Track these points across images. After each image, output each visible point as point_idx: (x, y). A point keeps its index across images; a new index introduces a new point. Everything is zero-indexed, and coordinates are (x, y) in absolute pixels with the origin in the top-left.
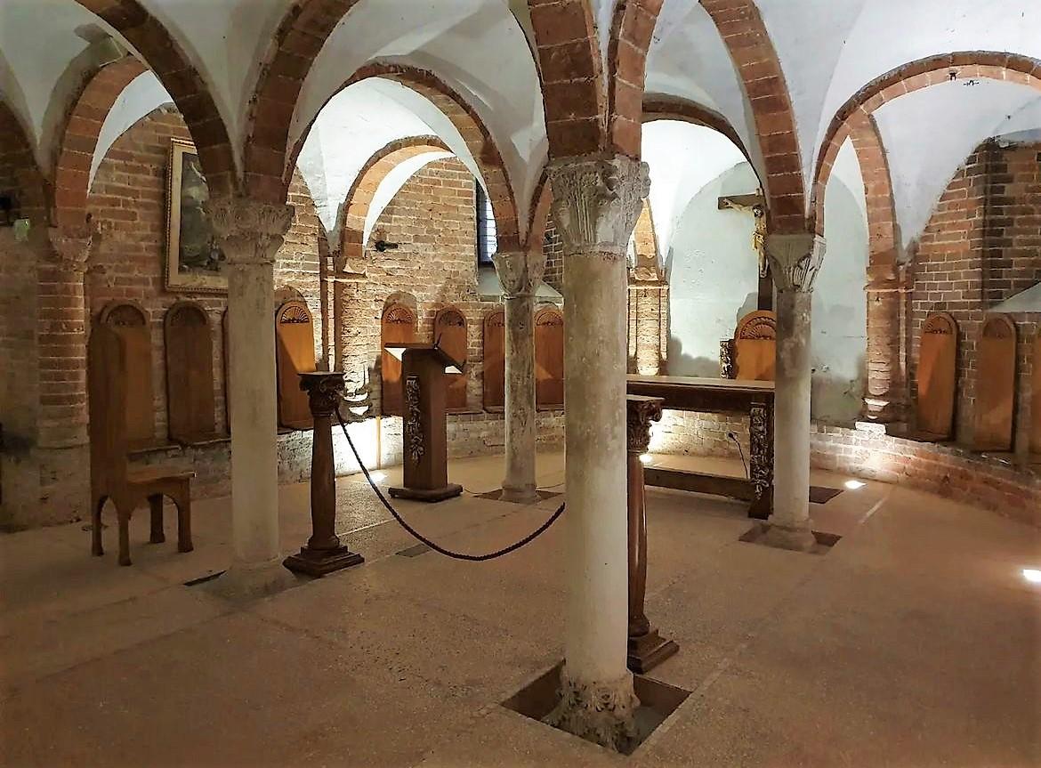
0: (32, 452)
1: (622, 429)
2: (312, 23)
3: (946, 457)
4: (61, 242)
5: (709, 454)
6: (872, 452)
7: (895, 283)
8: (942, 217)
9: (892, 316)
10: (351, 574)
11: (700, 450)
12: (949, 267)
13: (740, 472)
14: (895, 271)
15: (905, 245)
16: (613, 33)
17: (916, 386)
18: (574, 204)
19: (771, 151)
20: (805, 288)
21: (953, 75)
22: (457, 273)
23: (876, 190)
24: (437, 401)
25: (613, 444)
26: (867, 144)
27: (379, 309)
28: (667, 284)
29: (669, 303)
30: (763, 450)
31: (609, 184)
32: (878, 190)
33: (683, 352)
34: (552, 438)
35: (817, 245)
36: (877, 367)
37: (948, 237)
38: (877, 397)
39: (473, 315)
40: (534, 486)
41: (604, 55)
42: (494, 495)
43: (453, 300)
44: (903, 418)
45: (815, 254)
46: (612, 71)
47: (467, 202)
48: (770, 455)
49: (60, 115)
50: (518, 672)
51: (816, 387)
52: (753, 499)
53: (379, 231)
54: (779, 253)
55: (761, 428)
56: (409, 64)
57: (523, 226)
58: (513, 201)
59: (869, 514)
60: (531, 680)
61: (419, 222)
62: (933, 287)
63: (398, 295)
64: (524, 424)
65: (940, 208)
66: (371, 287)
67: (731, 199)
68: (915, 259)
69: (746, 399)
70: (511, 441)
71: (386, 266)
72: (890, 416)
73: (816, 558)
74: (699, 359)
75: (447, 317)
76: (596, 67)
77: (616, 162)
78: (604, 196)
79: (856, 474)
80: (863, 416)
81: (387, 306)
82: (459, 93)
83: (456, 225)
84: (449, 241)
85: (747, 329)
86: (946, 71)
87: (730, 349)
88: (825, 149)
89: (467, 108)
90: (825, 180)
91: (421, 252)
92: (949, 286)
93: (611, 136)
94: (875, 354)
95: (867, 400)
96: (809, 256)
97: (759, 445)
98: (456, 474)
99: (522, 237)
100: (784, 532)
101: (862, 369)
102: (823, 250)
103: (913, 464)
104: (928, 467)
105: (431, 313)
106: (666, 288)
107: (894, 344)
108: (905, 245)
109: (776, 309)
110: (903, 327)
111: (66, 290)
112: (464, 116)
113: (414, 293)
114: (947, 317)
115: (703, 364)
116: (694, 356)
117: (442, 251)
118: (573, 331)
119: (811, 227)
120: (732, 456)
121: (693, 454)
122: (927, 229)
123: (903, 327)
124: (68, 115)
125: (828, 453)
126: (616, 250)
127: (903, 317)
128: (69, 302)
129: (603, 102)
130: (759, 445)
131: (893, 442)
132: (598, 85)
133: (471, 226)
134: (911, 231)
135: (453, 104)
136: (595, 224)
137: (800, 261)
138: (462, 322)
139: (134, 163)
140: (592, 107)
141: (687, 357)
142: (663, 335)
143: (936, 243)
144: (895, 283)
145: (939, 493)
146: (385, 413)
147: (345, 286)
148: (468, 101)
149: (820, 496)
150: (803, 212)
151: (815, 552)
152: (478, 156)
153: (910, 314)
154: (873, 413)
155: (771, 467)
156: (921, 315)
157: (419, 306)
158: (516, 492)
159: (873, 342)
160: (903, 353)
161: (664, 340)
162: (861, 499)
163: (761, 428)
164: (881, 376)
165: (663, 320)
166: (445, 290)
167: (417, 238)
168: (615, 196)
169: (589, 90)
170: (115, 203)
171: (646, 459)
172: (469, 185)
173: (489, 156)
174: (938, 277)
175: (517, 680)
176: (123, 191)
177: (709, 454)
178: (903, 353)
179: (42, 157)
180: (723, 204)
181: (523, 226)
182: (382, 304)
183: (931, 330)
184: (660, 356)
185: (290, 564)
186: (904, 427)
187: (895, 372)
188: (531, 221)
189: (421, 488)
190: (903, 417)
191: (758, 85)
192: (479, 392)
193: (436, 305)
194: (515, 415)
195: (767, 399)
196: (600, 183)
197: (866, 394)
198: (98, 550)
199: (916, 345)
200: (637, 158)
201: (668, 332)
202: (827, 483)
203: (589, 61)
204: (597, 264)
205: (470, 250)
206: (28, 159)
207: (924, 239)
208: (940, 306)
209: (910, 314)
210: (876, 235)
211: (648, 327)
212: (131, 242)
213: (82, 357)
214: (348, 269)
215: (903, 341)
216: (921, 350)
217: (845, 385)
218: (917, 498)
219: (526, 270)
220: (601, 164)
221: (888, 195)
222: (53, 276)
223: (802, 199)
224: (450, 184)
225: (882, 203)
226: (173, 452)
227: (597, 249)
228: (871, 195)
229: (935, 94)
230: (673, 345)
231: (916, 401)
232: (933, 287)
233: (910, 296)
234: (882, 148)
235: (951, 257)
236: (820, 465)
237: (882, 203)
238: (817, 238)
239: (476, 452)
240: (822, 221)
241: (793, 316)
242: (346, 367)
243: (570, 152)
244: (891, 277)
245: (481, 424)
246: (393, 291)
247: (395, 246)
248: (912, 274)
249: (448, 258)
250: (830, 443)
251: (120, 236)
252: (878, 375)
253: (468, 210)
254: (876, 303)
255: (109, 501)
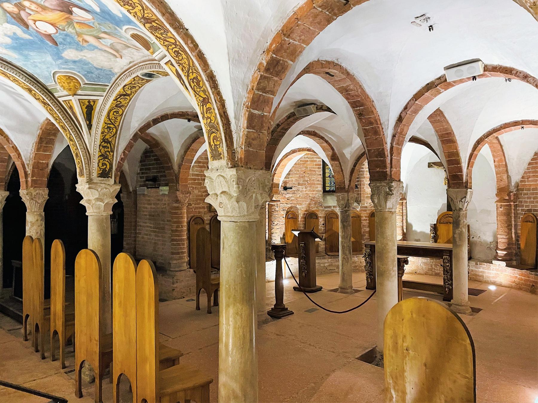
0: (168, 272)
1: (396, 268)
2: (283, 129)
3: (532, 276)
4: (180, 195)
5: (426, 274)
6: (500, 275)
7: (509, 201)
8: (529, 172)
9: (508, 214)
10: (290, 317)
11: (422, 272)
12: (533, 194)
13: (440, 282)
14: (509, 195)
15: (513, 184)
16: (391, 144)
17: (519, 245)
18: (379, 196)
19: (449, 157)
20: (464, 209)
21: (522, 127)
22: (314, 198)
23: (498, 162)
24: (312, 252)
25: (393, 274)
26: (494, 143)
27: (284, 213)
28: (406, 199)
29: (406, 208)
30: (448, 273)
31: (391, 191)
32: (500, 161)
33: (414, 229)
34: (356, 266)
35: (469, 193)
36: (502, 236)
37: (533, 181)
38: (502, 250)
39: (321, 214)
40: (352, 287)
41: (389, 151)
42: (335, 290)
43: (314, 209)
44: (513, 259)
45: (468, 196)
46: (391, 155)
47: (319, 168)
48: (451, 275)
49: (183, 152)
50: (361, 350)
51: (471, 245)
52: (445, 293)
53: (285, 182)
54: (453, 196)
55: (448, 264)
56: (307, 130)
57: (347, 183)
58: (343, 174)
59: (496, 301)
60: (365, 352)
61: (300, 177)
62: (526, 202)
63: (291, 208)
64: (348, 262)
65: (528, 169)
66: (281, 205)
67: (433, 163)
68: (518, 190)
69: (446, 245)
70: (342, 269)
71: (287, 196)
72: (508, 258)
73: (471, 317)
74: (421, 232)
75: (311, 216)
76: (386, 155)
77: (393, 184)
78: (389, 194)
79: (494, 283)
80: (496, 258)
81: (287, 212)
82: (324, 136)
83: (314, 178)
84: (311, 185)
85: (442, 219)
86: (520, 127)
87: (435, 228)
88: (471, 156)
89: (327, 142)
90: (472, 167)
91: (301, 189)
92: (533, 202)
93: (391, 175)
94: (501, 231)
95: (498, 251)
96: (465, 197)
97: (447, 271)
98: (319, 282)
99: (347, 187)
100: (458, 307)
101: (495, 237)
102: (472, 193)
103: (519, 279)
104: (525, 280)
105: (304, 214)
106: (405, 201)
107: (509, 227)
108: (513, 184)
109: (452, 216)
110: (513, 219)
111: (182, 212)
112: (325, 144)
113: (298, 206)
114: (532, 215)
115: (423, 234)
116: (419, 231)
117: (309, 189)
118: (379, 236)
119: (467, 186)
120: (437, 275)
121: (419, 274)
122: (523, 177)
123: (513, 219)
124: (186, 152)
125: (481, 274)
126: (393, 210)
127: (513, 215)
128: (182, 218)
129: (388, 166)
130: (447, 271)
131: (509, 270)
132: (387, 160)
133: (320, 178)
134: (516, 178)
135: (322, 141)
136: (386, 203)
137: (462, 199)
138: (317, 217)
139: (201, 165)
140: (385, 167)
141: (415, 231)
142: (404, 222)
143: (527, 183)
144: (509, 201)
145: (530, 292)
146: (8, 191)
147: (272, 205)
148: (327, 139)
149: (473, 292)
150: (462, 180)
151: (471, 315)
152: (329, 158)
153: (516, 215)
154: (500, 257)
155: (452, 280)
156: (521, 214)
157: (299, 211)
158: (345, 289)
159: (500, 226)
160: (513, 231)
161: (405, 224)
162: (497, 294)
163: (448, 264)
164: (504, 240)
165: (404, 215)
166: (310, 204)
167: (299, 184)
168: (393, 194)
169: (384, 162)
170: (195, 180)
171: (405, 278)
172: (319, 161)
173: (334, 157)
174: (528, 198)
175: (360, 353)
176: (197, 175)
177: (426, 274)
178: (513, 231)
179: (176, 167)
180: (430, 165)
181: (347, 183)
182: (285, 211)
183: (525, 221)
184: (403, 230)
185: (269, 313)
186: (514, 263)
187: (510, 238)
188: (350, 181)
189: (307, 287)
190: (514, 258)
191: (443, 134)
192: (324, 247)
193: (306, 211)
194: (344, 258)
195: (450, 252)
196: (388, 190)
197: (497, 248)
198: (198, 308)
199: (519, 227)
200: (400, 181)
201: (407, 220)
202: (476, 286)
203: (384, 154)
204: (387, 215)
205: (320, 188)
206: (171, 168)
207: (521, 181)
208: (529, 211)
209: (516, 215)
210: (499, 180)
211: (398, 218)
212: (200, 194)
213: (185, 237)
214: (274, 199)
215: (513, 225)
216: (521, 229)
217: (488, 244)
218: (520, 293)
219: (348, 200)
220: (388, 184)
221: (504, 163)
222: (177, 208)
223: (462, 175)
224: (312, 161)
225: (502, 167)
226: (214, 272)
227: (387, 210)
228: (496, 163)
229: (517, 132)
230: (409, 226)
231: (520, 252)
232: (526, 202)
233: (516, 206)
234: (501, 145)
235: (533, 189)
236: (473, 278)
237: (502, 167)
238: (469, 190)
239: (328, 271)
240: (471, 183)
241: (460, 221)
242: (273, 238)
243: (377, 180)
244: (507, 198)
245: (326, 261)
246: (290, 206)
247: (291, 188)
248: (517, 196)
249: (311, 191)
250: (481, 270)
251: (196, 192)
252: (502, 240)
253: (319, 171)
254: (501, 209)
255: (202, 289)
